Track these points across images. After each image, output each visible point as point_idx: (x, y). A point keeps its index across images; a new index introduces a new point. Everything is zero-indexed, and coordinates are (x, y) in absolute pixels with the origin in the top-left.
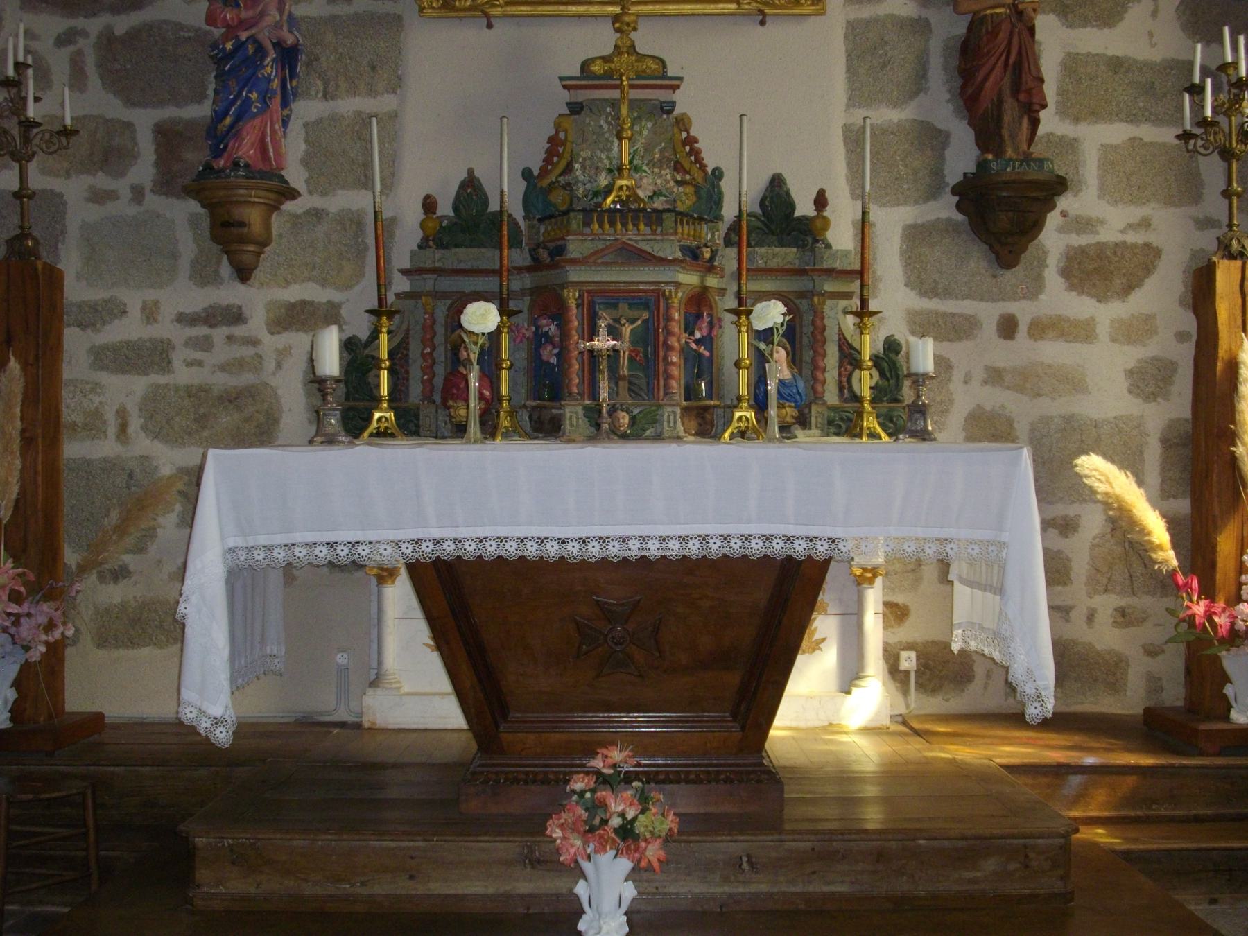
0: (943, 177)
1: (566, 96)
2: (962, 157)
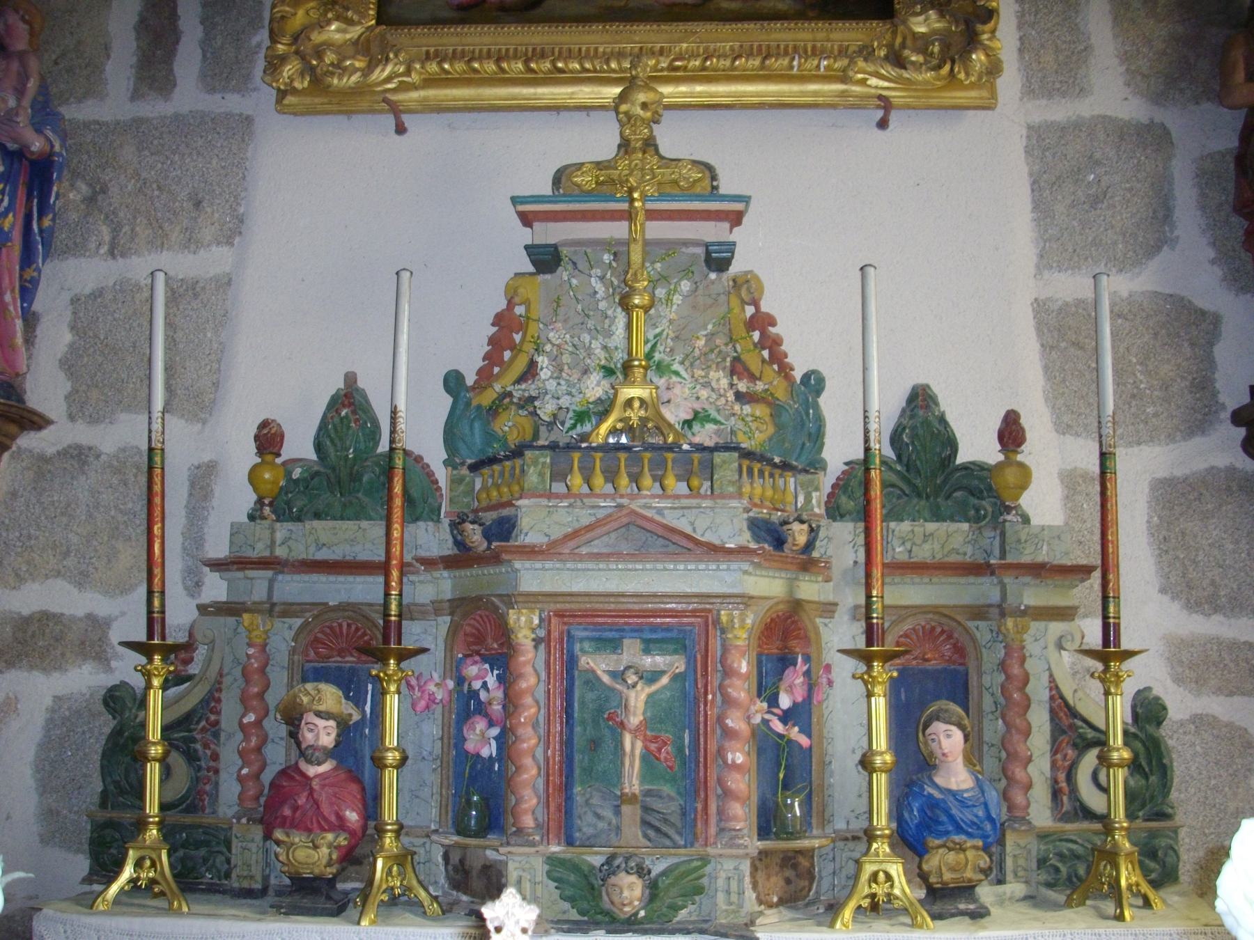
0: (1215, 394)
1: (526, 236)
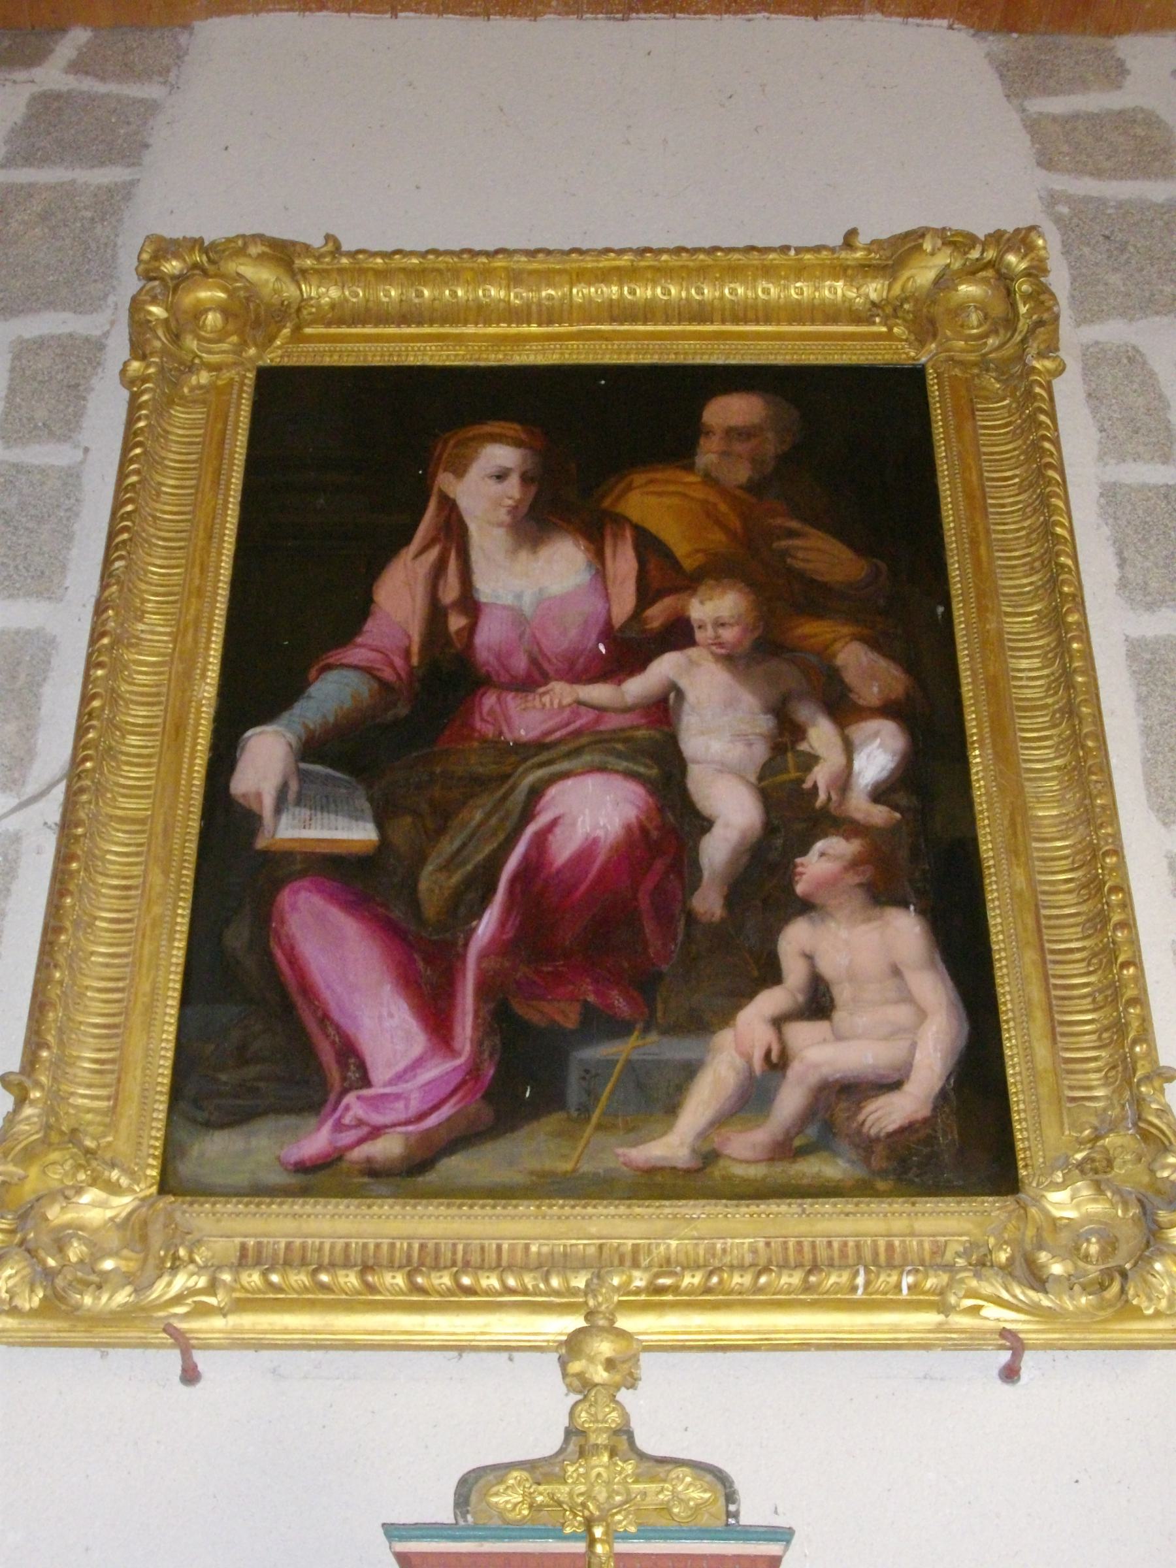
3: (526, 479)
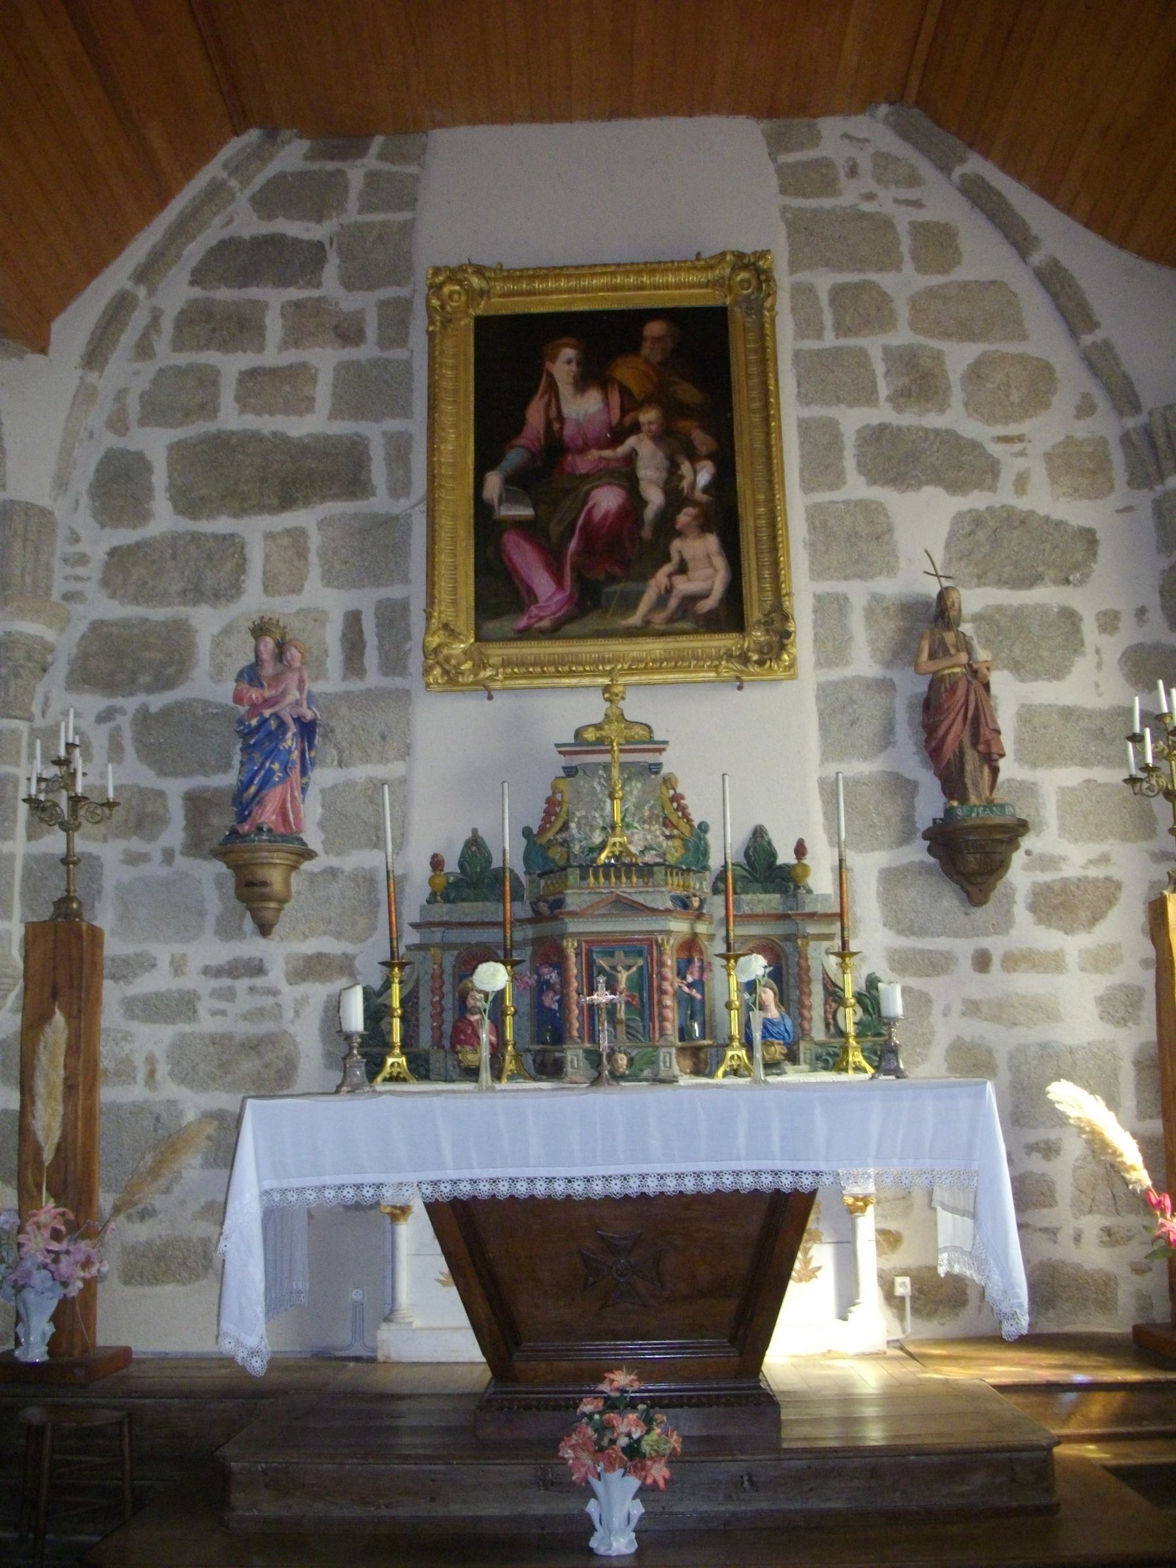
0: (914, 823)
1: (563, 761)
2: (930, 804)
3: (578, 364)
